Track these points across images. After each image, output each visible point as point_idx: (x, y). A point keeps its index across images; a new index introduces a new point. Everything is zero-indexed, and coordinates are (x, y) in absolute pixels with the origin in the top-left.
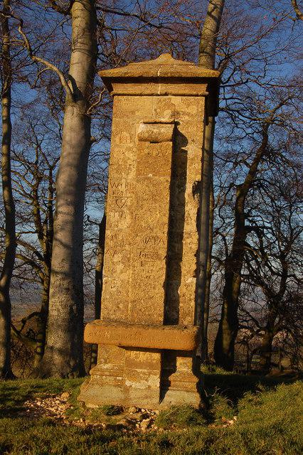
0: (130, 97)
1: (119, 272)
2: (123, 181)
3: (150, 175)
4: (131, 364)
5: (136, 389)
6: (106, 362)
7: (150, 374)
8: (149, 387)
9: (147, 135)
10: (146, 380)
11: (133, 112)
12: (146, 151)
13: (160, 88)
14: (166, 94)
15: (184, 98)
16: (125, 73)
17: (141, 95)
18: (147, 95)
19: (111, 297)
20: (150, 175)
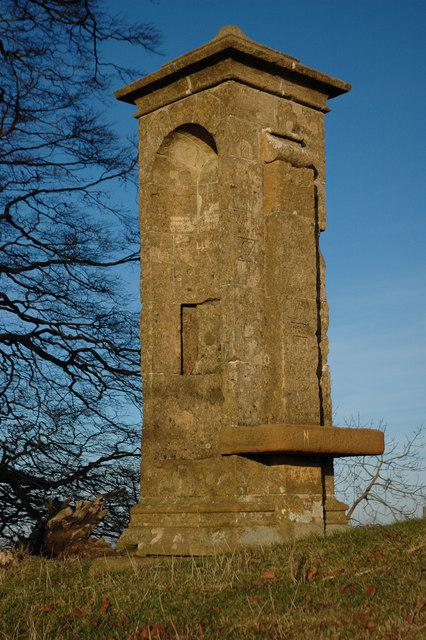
0: (249, 89)
1: (251, 352)
2: (249, 215)
3: (295, 213)
4: (292, 487)
5: (301, 524)
6: (246, 494)
7: (313, 499)
8: (313, 518)
9: (288, 153)
10: (310, 510)
11: (253, 113)
12: (289, 176)
13: (282, 86)
14: (288, 97)
15: (306, 108)
16: (260, 53)
17: (262, 89)
18: (268, 92)
19: (245, 392)
20: (295, 213)
